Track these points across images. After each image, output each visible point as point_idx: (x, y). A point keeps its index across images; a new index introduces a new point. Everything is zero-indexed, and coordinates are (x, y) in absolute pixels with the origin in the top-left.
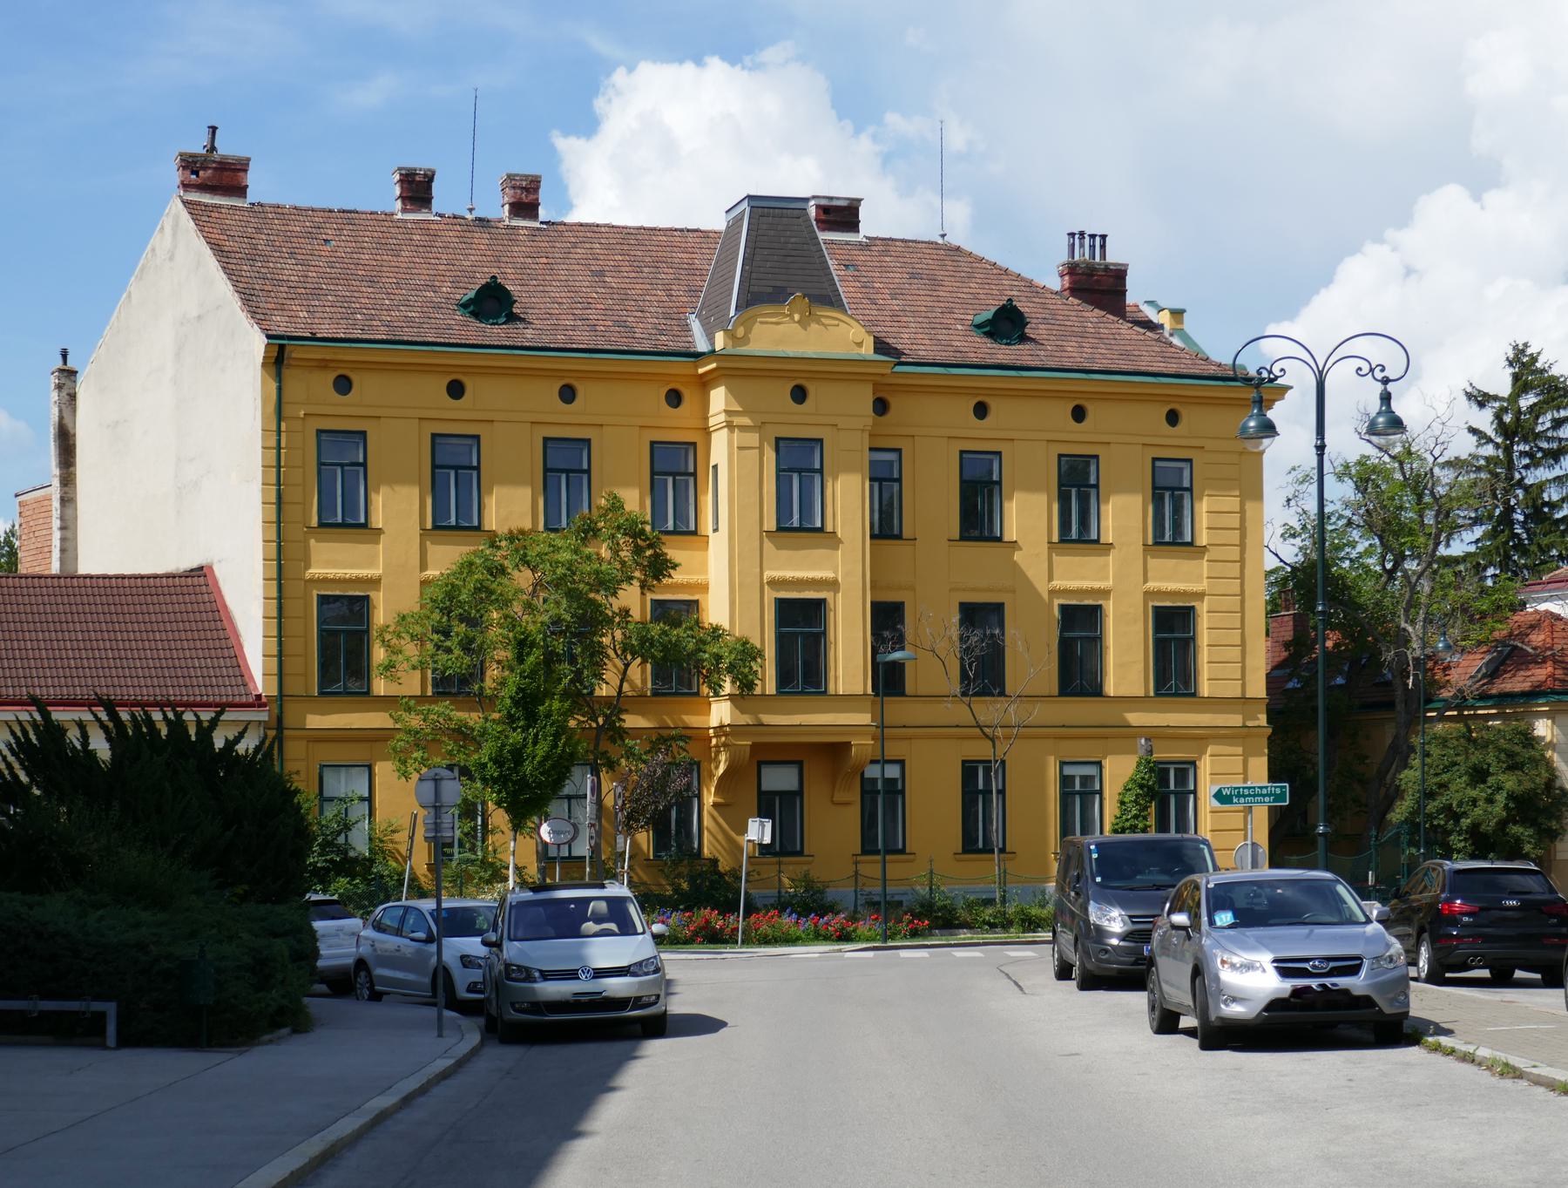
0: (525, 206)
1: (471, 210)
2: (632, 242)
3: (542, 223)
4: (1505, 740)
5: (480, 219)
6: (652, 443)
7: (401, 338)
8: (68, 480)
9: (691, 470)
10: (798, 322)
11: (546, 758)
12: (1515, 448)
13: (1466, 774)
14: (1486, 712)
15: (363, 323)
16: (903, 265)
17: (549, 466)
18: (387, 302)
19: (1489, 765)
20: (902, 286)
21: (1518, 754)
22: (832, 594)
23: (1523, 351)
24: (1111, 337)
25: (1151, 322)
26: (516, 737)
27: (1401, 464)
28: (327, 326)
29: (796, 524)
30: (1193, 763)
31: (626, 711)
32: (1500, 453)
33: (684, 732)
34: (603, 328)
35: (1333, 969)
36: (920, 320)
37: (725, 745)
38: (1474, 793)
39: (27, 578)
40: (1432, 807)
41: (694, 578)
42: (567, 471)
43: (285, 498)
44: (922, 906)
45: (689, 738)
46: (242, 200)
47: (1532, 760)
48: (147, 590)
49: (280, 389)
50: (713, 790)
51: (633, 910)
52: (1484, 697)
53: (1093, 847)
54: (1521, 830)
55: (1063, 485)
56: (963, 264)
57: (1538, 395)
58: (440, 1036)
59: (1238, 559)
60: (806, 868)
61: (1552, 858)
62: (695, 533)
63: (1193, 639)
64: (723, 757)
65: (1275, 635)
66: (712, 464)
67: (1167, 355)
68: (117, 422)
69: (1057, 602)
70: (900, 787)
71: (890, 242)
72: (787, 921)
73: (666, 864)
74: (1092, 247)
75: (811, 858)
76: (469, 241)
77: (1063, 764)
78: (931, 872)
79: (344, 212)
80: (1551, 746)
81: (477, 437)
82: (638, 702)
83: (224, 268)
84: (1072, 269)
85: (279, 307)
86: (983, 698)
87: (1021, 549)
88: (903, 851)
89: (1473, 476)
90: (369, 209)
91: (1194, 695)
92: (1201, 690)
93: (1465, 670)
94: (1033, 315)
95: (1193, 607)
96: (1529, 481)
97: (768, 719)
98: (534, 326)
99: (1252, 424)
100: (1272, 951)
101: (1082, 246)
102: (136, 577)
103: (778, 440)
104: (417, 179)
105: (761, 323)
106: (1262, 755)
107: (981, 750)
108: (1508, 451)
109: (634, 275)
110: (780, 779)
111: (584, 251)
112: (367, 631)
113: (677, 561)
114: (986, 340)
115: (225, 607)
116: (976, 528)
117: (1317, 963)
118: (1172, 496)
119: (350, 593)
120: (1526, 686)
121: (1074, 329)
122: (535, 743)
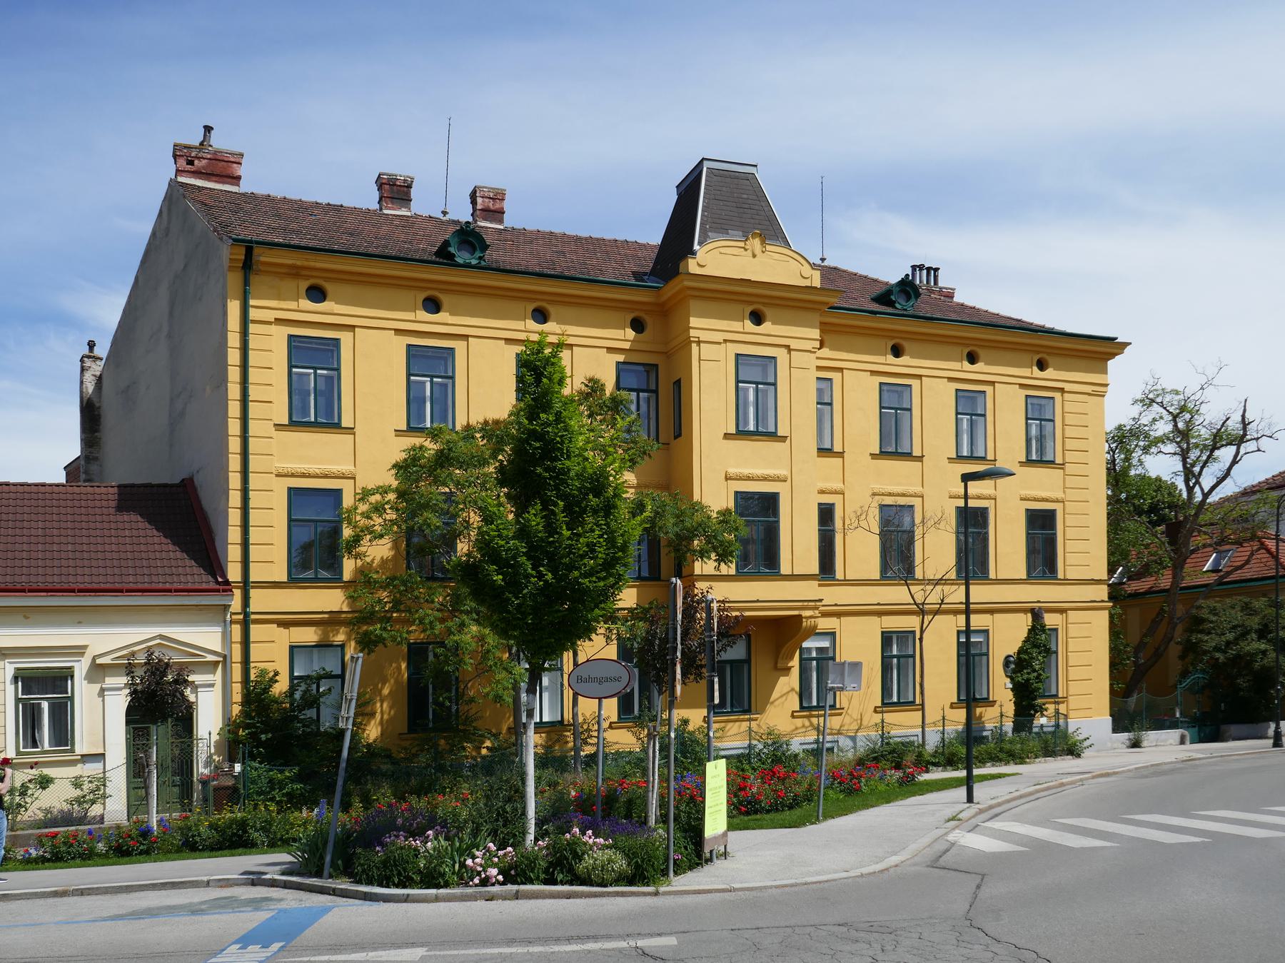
68: (129, 386)
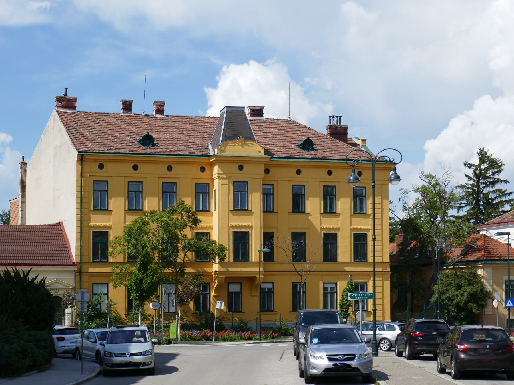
0: (160, 110)
1: (144, 112)
2: (193, 121)
3: (165, 116)
4: (468, 275)
5: (146, 115)
6: (196, 183)
7: (119, 152)
8: (23, 196)
9: (208, 192)
10: (241, 145)
11: (150, 283)
12: (480, 181)
13: (454, 287)
14: (462, 266)
15: (108, 147)
16: (276, 127)
17: (163, 191)
18: (116, 141)
19: (462, 284)
20: (276, 133)
21: (472, 280)
22: (251, 230)
23: (482, 151)
24: (341, 148)
25: (356, 143)
26: (141, 276)
27: (434, 188)
28: (97, 149)
29: (240, 208)
30: (366, 283)
31: (186, 267)
32: (475, 183)
33: (203, 273)
34: (181, 148)
35: (346, 358)
36: (280, 144)
37: (217, 277)
38: (457, 293)
39: (11, 226)
40: (443, 297)
41: (208, 225)
42: (169, 192)
43: (83, 201)
44: (278, 328)
45: (204, 275)
46: (74, 110)
47: (476, 282)
48: (43, 230)
49: (82, 168)
50: (214, 291)
51: (147, 334)
52: (461, 262)
53: (302, 314)
54: (472, 305)
55: (325, 195)
56: (295, 126)
57: (487, 164)
58: (82, 374)
59: (381, 218)
60: (241, 316)
61: (483, 313)
62: (209, 211)
63: (366, 243)
64: (216, 281)
65: (397, 242)
66: (214, 190)
67: (358, 154)
68: (38, 178)
69: (323, 232)
70: (272, 291)
71: (273, 120)
72: (232, 334)
73: (198, 315)
74: (337, 120)
75: (244, 313)
76: (142, 122)
77: (324, 283)
78: (281, 318)
79: (105, 113)
80: (483, 277)
81: (142, 182)
82: (190, 264)
83: (67, 131)
84: (330, 127)
85: (83, 143)
86: (297, 263)
87: (311, 215)
88: (273, 311)
89: (467, 190)
90: (113, 112)
91: (366, 261)
92: (369, 260)
93: (456, 253)
94: (317, 142)
95: (366, 234)
96: (484, 192)
97: (230, 269)
98: (160, 148)
99: (352, 178)
100: (326, 352)
101: (333, 120)
102: (39, 226)
103: (234, 182)
104: (127, 103)
105: (229, 146)
106: (388, 280)
107: (297, 279)
108: (478, 182)
109: (192, 131)
110: (234, 288)
111: (177, 124)
112: (107, 242)
113: (201, 220)
114: (301, 150)
115: (66, 235)
116: (297, 209)
117: (340, 356)
118: (359, 198)
119: (102, 230)
120: (475, 258)
121: (329, 146)
122: (147, 278)
